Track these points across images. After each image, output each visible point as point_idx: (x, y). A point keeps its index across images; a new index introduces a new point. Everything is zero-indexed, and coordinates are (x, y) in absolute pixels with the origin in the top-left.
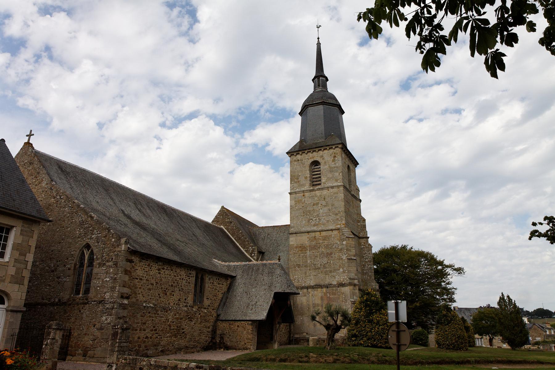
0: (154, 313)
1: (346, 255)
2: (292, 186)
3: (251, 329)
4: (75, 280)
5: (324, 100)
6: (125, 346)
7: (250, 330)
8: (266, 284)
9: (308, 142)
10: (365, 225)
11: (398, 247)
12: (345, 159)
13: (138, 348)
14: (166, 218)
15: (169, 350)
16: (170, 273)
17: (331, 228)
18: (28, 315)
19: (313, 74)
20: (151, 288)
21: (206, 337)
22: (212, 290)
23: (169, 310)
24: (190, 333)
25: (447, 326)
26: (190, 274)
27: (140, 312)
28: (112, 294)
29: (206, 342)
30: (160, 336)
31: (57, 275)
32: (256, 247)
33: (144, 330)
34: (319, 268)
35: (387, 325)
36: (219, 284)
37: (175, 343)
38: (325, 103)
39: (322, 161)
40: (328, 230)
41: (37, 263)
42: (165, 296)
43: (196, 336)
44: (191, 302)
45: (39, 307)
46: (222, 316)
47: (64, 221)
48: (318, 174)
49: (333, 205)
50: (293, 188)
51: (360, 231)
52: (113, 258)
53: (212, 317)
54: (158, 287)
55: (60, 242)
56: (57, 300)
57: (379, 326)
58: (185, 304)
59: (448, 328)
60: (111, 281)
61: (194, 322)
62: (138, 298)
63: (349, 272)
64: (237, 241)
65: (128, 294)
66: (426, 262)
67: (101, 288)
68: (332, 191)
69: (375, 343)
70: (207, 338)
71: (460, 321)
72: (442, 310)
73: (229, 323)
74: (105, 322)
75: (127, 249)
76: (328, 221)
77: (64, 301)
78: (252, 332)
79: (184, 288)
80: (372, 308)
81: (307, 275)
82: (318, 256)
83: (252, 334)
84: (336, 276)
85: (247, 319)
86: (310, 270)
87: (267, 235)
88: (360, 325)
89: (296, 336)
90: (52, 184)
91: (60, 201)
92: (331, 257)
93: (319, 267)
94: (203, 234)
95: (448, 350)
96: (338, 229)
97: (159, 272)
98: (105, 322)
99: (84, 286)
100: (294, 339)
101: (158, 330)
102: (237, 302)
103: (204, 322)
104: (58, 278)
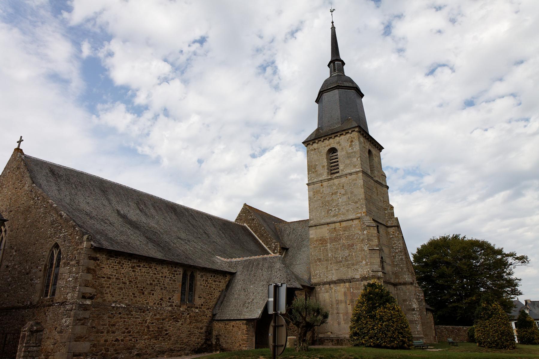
3: (246, 329)
4: (45, 282)
7: (244, 330)
10: (394, 213)
11: (450, 237)
12: (365, 143)
13: (104, 352)
14: (174, 217)
15: (147, 354)
16: (148, 271)
17: (351, 217)
18: (5, 319)
19: (329, 59)
20: (123, 287)
21: (198, 338)
22: (206, 288)
24: (175, 334)
25: (488, 321)
26: (176, 271)
27: (107, 313)
28: (73, 294)
29: (198, 344)
30: (136, 338)
32: (278, 243)
33: (114, 332)
35: (392, 321)
36: (215, 281)
37: (156, 346)
39: (339, 147)
42: (143, 295)
43: (184, 338)
44: (177, 302)
47: (39, 222)
49: (352, 193)
50: (311, 178)
51: (388, 219)
52: (76, 257)
53: (205, 317)
54: (132, 286)
55: (35, 244)
57: (383, 322)
59: (489, 323)
62: (105, 298)
64: (260, 239)
65: (92, 294)
66: (483, 251)
67: (64, 289)
70: (199, 340)
71: (503, 315)
72: (481, 303)
73: (224, 323)
76: (348, 211)
79: (168, 287)
80: (375, 302)
81: (329, 269)
84: (359, 269)
85: (242, 318)
86: (331, 264)
87: (292, 230)
88: (361, 321)
89: (320, 336)
90: (33, 186)
92: (353, 249)
93: (341, 260)
95: (490, 349)
97: (133, 269)
98: (64, 325)
99: (52, 287)
100: (319, 339)
101: (132, 332)
102: (234, 301)
103: (195, 323)
104: (32, 280)
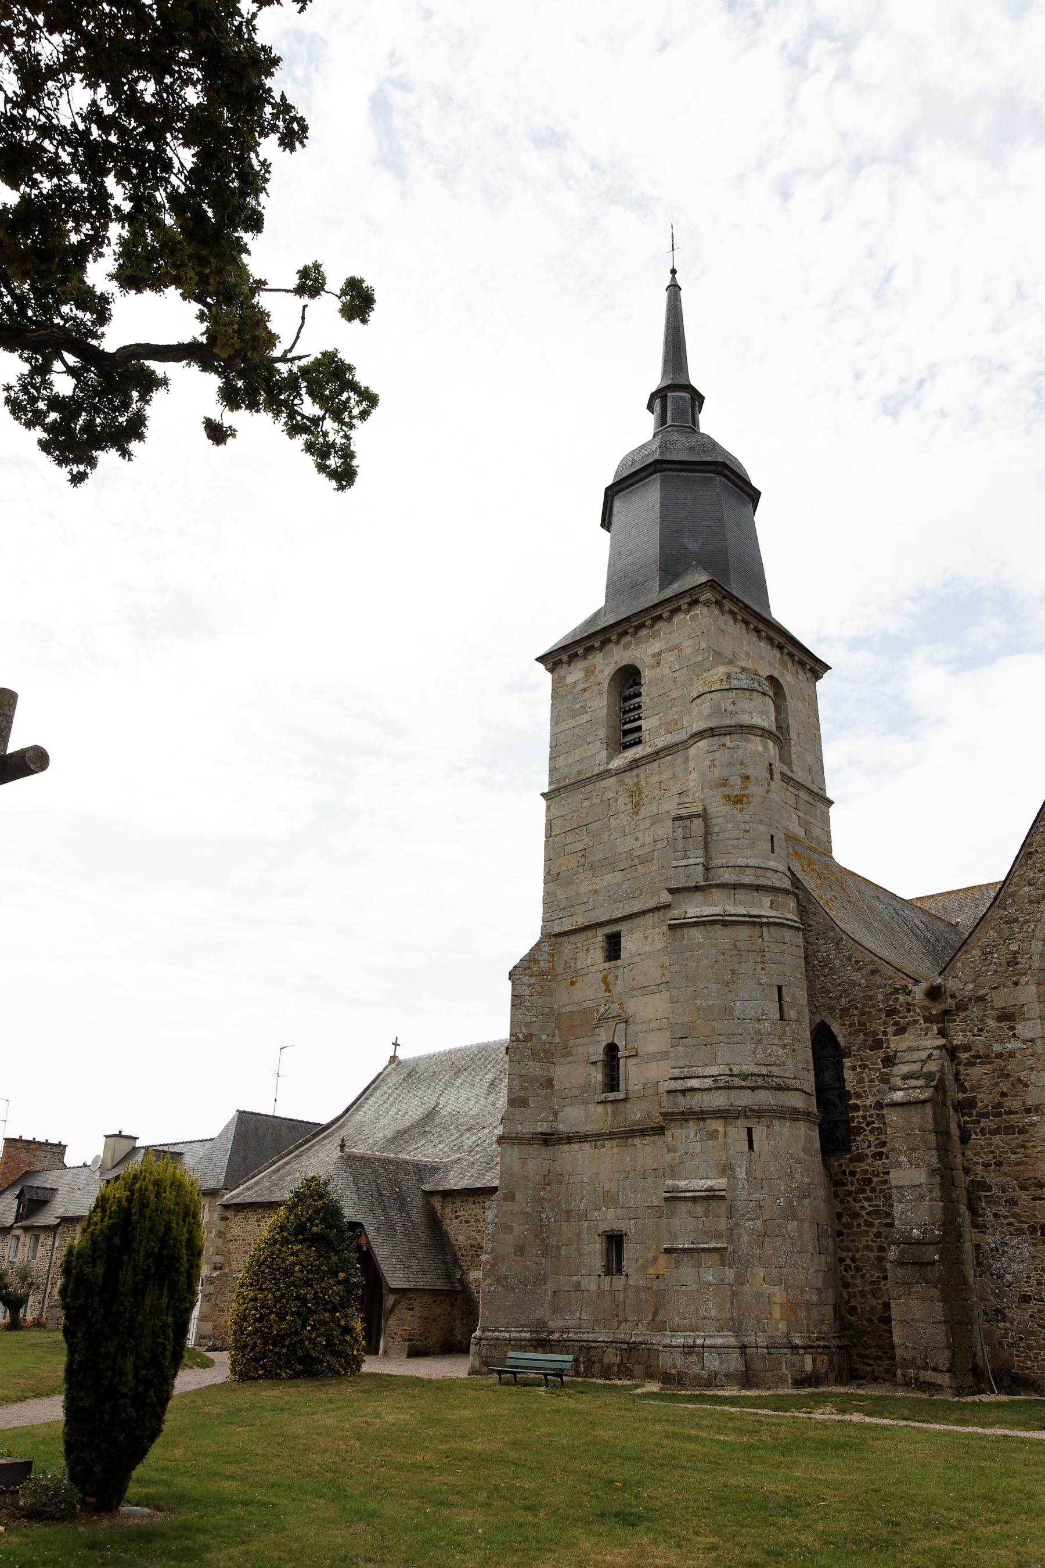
19: (654, 379)
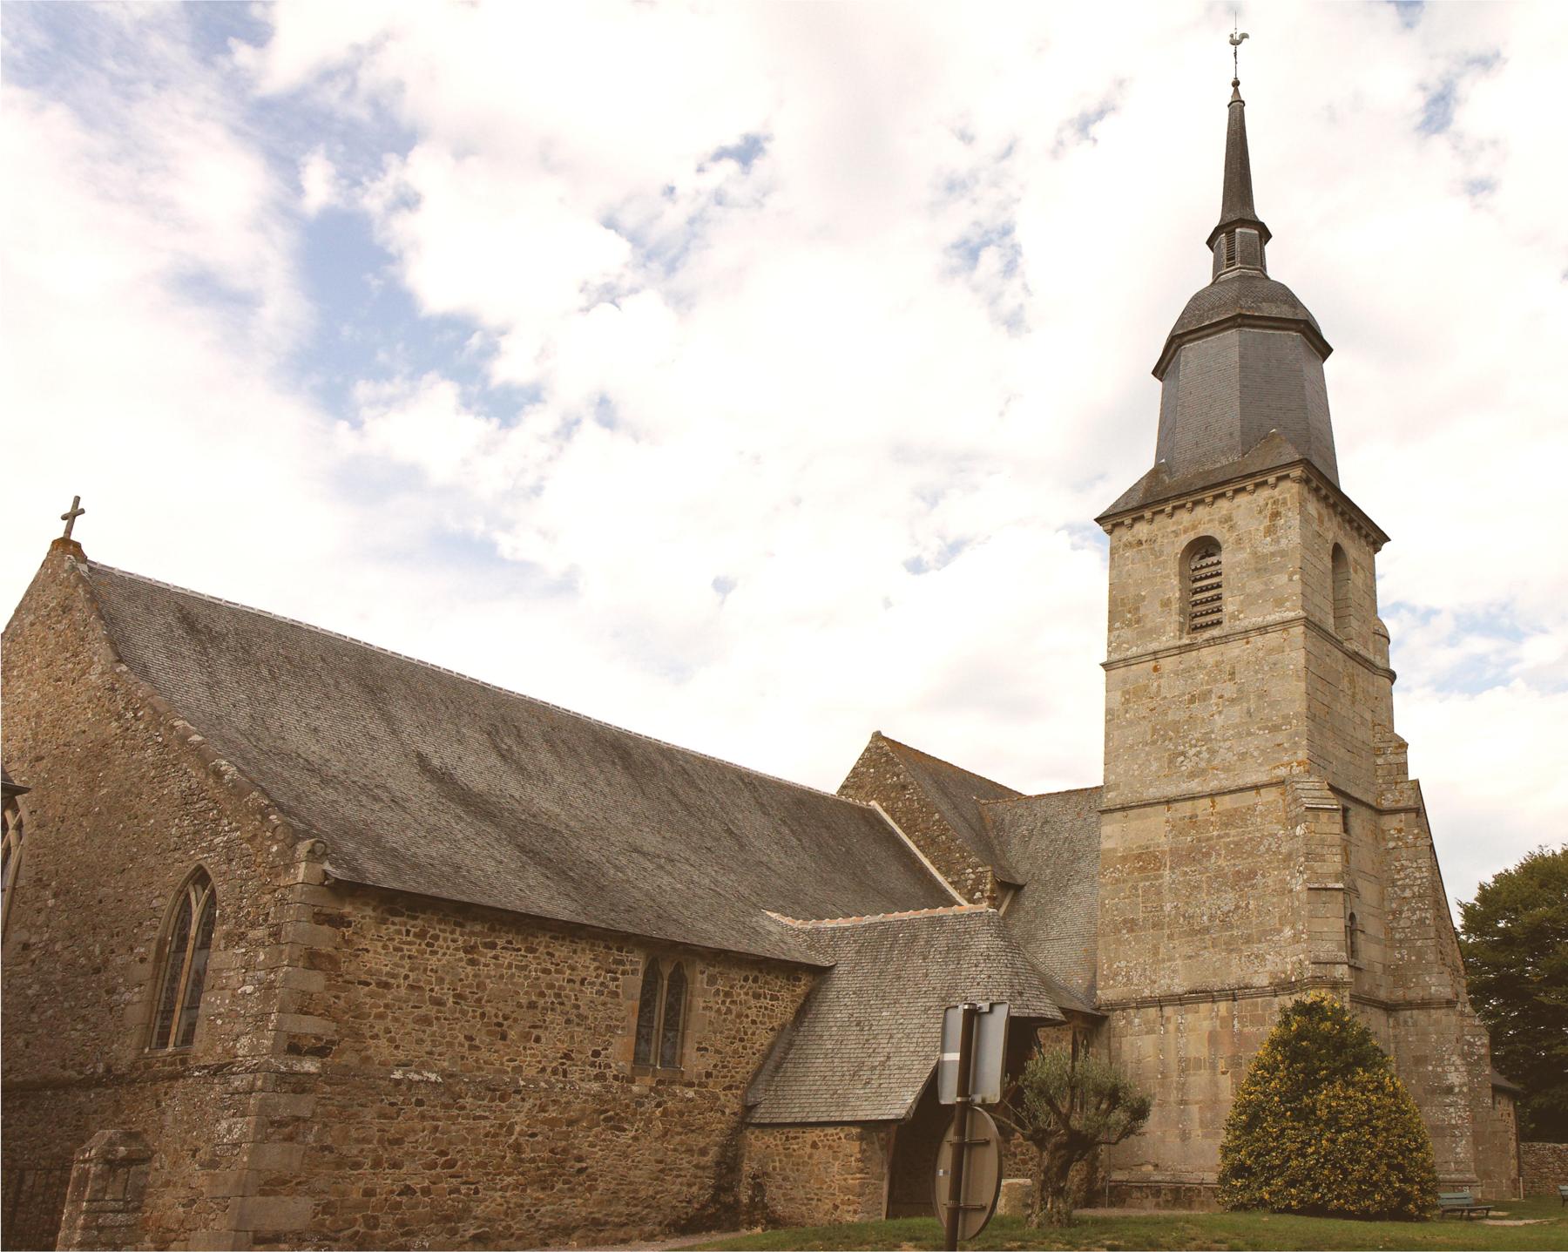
0: (442, 1104)
1: (1305, 877)
2: (1112, 639)
3: (859, 1156)
5: (1241, 308)
6: (120, 1226)
7: (853, 1159)
8: (934, 989)
9: (1177, 471)
10: (1406, 763)
13: (362, 1231)
15: (512, 1235)
20: (433, 1014)
21: (690, 1185)
22: (725, 1020)
23: (515, 1092)
24: (611, 1172)
26: (621, 962)
28: (258, 1040)
31: (107, 981)
32: (989, 868)
33: (396, 1165)
34: (1207, 930)
36: (757, 996)
37: (543, 1210)
38: (1246, 321)
40: (1241, 790)
41: (58, 947)
42: (501, 1042)
43: (643, 1183)
45: (49, 1093)
46: (763, 1111)
47: (139, 795)
48: (1213, 587)
49: (1263, 694)
50: (1119, 646)
51: (1384, 786)
52: (268, 913)
53: (719, 1115)
54: (464, 1013)
56: (101, 1069)
57: (1339, 1132)
58: (596, 1071)
60: (257, 994)
61: (633, 1133)
62: (369, 1052)
63: (1314, 937)
65: (322, 1040)
68: (1260, 645)
69: (1317, 1195)
70: (695, 1189)
73: (783, 1133)
74: (225, 1140)
75: (321, 878)
76: (1243, 756)
77: (119, 1072)
78: (860, 1164)
80: (1318, 1064)
81: (1160, 956)
82: (1205, 886)
83: (861, 1171)
84: (1268, 957)
87: (1039, 824)
89: (1117, 1176)
91: (133, 728)
93: (1207, 923)
94: (775, 829)
96: (1280, 783)
98: (225, 1140)
101: (460, 1163)
102: (821, 1060)
103: (680, 1134)
